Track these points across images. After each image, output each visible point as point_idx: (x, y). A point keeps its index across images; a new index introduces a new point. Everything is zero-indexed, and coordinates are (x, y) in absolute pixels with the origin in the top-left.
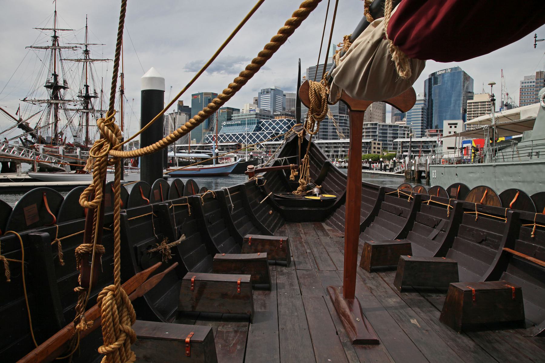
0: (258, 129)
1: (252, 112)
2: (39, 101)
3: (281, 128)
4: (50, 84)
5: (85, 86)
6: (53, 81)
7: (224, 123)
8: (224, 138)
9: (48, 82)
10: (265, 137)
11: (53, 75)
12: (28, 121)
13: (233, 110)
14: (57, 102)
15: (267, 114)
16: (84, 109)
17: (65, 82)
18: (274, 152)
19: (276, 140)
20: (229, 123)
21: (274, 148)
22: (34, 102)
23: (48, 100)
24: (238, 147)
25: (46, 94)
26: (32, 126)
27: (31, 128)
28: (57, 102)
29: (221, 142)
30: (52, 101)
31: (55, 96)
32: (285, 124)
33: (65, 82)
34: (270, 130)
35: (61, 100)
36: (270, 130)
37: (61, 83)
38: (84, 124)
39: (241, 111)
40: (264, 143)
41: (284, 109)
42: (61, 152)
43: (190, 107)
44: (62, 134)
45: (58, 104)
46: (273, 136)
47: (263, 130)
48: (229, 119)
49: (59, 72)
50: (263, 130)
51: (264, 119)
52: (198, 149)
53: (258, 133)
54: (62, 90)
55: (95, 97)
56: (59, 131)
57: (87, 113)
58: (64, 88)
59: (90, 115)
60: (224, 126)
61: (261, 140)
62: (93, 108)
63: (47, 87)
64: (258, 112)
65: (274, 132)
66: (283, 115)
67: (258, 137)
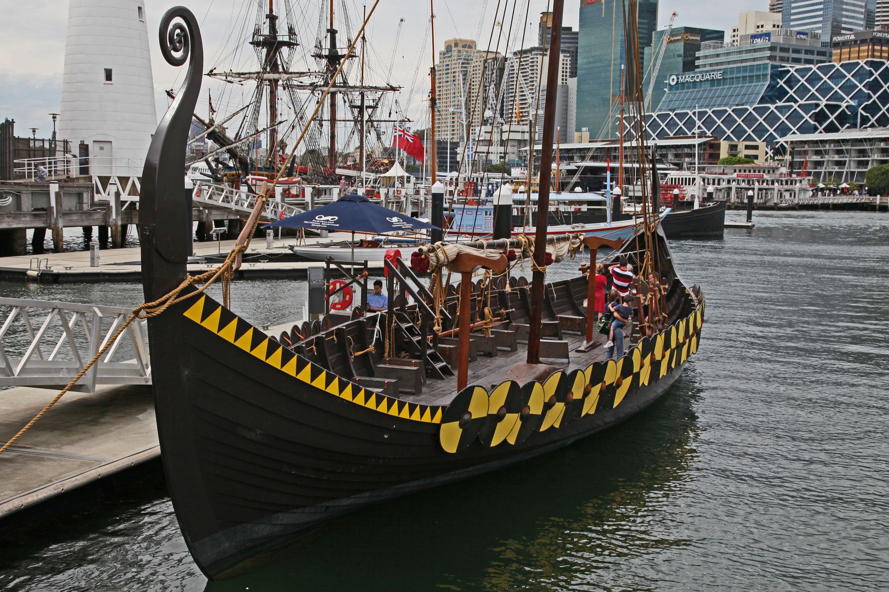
0: (775, 94)
1: (759, 42)
2: (239, 74)
3: (848, 88)
4: (261, 38)
5: (328, 31)
6: (266, 31)
7: (672, 80)
8: (671, 124)
9: (257, 32)
10: (795, 117)
11: (267, 17)
12: (225, 126)
13: (706, 35)
14: (276, 76)
15: (808, 43)
16: (326, 84)
17: (291, 31)
18: (818, 164)
19: (831, 128)
20: (687, 78)
21: (818, 153)
22: (229, 79)
23: (258, 73)
24: (710, 152)
25: (252, 60)
26: (230, 134)
27: (228, 139)
28: (276, 76)
29: (662, 135)
30: (266, 76)
31: (272, 64)
32: (861, 75)
33: (291, 31)
34: (813, 97)
35: (285, 72)
36: (813, 97)
37: (283, 35)
38: (327, 115)
39: (727, 39)
40: (790, 138)
41: (870, 20)
42: (516, 273)
43: (576, 29)
44: (283, 145)
45: (278, 81)
46: (820, 117)
47: (791, 99)
48: (689, 65)
49: (279, 10)
50: (791, 99)
51: (797, 61)
52: (594, 158)
53: (772, 107)
54: (285, 50)
55: (351, 56)
56: (280, 137)
57: (333, 94)
58: (289, 45)
59: (339, 97)
60: (671, 87)
61: (783, 130)
62: (345, 82)
63: (256, 44)
64: (781, 40)
65: (823, 102)
66: (863, 42)
67: (772, 119)
